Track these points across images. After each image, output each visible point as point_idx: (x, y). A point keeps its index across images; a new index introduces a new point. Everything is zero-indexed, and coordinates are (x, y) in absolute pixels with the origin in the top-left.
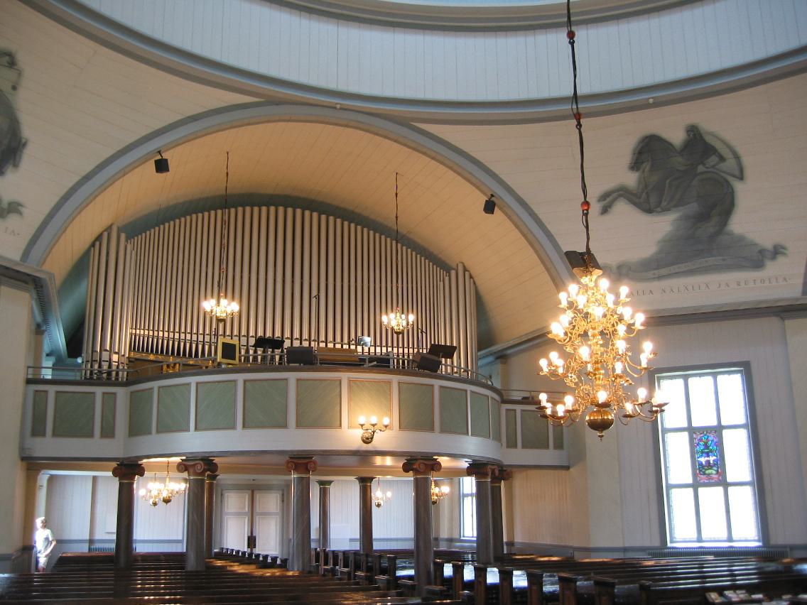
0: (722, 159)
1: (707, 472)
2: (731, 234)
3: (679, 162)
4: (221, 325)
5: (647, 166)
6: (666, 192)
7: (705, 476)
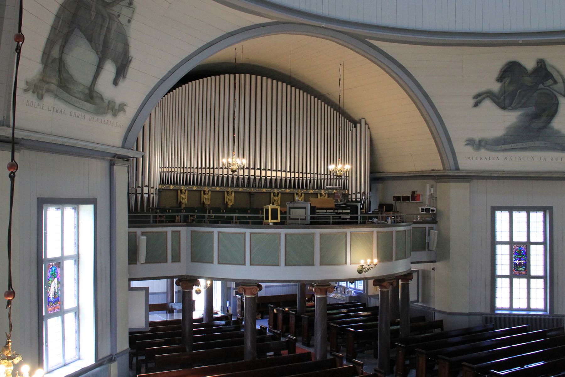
0: (555, 82)
1: (519, 269)
2: (552, 129)
3: (528, 80)
5: (508, 80)
6: (516, 97)
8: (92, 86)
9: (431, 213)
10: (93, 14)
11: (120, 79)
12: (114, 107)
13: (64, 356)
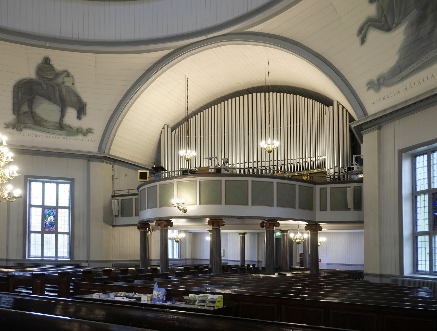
8: (61, 122)
9: (351, 171)
10: (45, 86)
11: (82, 115)
12: (82, 131)
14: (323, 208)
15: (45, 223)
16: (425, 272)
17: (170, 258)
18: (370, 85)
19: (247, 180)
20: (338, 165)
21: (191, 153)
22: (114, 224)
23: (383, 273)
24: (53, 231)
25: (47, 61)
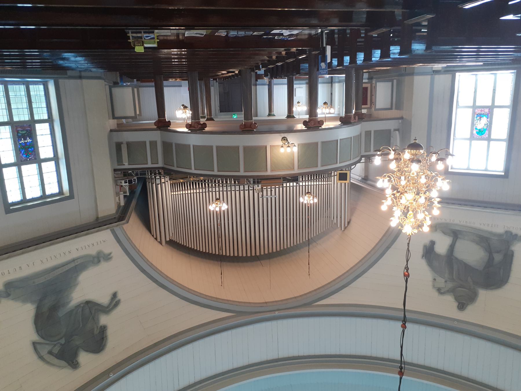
0: (50, 353)
2: (32, 302)
3: (77, 341)
4: (218, 197)
7: (26, 129)
9: (127, 180)
13: (476, 81)
14: (153, 144)
15: (489, 119)
16: (20, 83)
17: (152, 86)
18: (109, 257)
19: (245, 173)
20: (157, 186)
21: (306, 200)
22: (400, 121)
23: (79, 80)
24: (479, 109)
25: (462, 307)
